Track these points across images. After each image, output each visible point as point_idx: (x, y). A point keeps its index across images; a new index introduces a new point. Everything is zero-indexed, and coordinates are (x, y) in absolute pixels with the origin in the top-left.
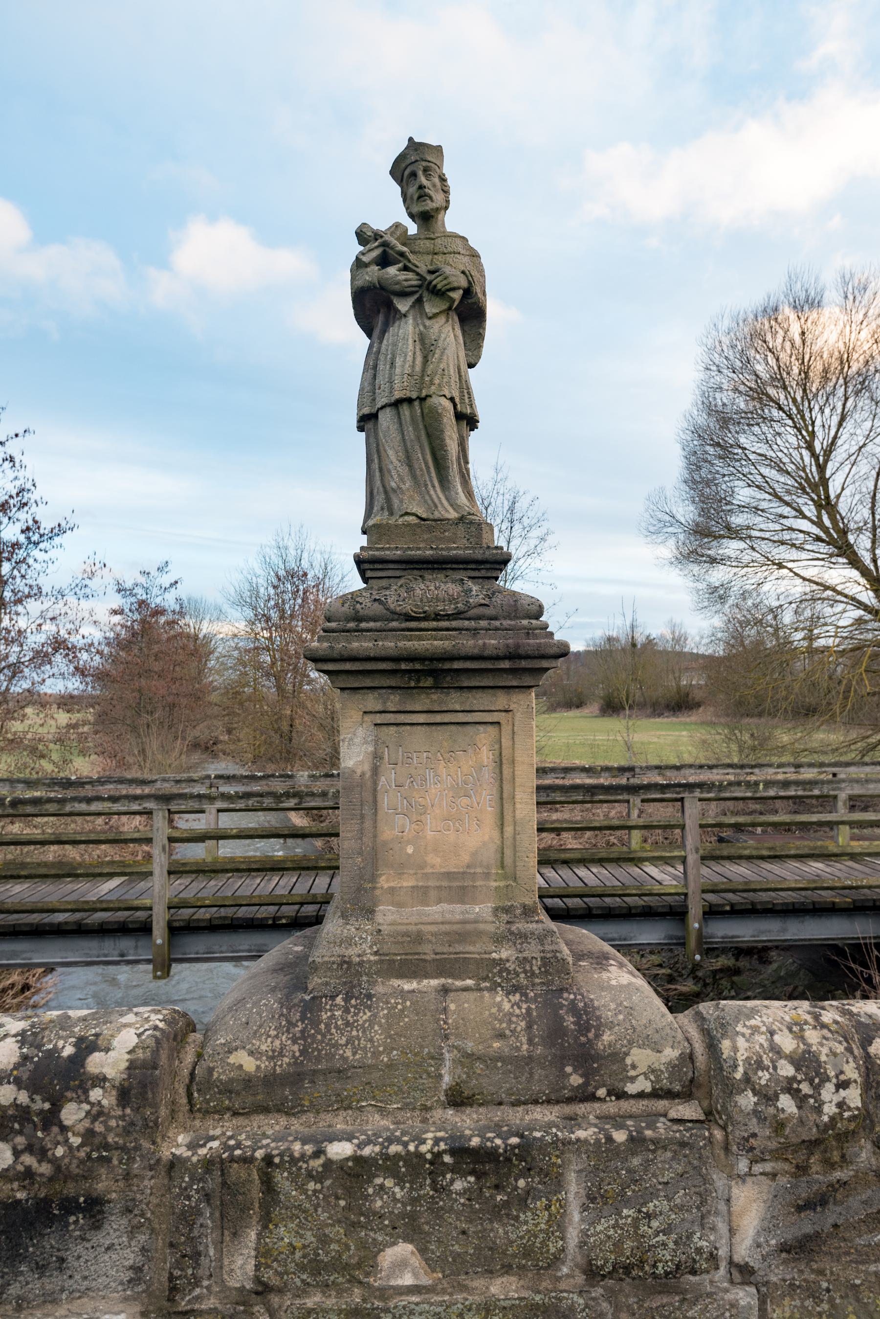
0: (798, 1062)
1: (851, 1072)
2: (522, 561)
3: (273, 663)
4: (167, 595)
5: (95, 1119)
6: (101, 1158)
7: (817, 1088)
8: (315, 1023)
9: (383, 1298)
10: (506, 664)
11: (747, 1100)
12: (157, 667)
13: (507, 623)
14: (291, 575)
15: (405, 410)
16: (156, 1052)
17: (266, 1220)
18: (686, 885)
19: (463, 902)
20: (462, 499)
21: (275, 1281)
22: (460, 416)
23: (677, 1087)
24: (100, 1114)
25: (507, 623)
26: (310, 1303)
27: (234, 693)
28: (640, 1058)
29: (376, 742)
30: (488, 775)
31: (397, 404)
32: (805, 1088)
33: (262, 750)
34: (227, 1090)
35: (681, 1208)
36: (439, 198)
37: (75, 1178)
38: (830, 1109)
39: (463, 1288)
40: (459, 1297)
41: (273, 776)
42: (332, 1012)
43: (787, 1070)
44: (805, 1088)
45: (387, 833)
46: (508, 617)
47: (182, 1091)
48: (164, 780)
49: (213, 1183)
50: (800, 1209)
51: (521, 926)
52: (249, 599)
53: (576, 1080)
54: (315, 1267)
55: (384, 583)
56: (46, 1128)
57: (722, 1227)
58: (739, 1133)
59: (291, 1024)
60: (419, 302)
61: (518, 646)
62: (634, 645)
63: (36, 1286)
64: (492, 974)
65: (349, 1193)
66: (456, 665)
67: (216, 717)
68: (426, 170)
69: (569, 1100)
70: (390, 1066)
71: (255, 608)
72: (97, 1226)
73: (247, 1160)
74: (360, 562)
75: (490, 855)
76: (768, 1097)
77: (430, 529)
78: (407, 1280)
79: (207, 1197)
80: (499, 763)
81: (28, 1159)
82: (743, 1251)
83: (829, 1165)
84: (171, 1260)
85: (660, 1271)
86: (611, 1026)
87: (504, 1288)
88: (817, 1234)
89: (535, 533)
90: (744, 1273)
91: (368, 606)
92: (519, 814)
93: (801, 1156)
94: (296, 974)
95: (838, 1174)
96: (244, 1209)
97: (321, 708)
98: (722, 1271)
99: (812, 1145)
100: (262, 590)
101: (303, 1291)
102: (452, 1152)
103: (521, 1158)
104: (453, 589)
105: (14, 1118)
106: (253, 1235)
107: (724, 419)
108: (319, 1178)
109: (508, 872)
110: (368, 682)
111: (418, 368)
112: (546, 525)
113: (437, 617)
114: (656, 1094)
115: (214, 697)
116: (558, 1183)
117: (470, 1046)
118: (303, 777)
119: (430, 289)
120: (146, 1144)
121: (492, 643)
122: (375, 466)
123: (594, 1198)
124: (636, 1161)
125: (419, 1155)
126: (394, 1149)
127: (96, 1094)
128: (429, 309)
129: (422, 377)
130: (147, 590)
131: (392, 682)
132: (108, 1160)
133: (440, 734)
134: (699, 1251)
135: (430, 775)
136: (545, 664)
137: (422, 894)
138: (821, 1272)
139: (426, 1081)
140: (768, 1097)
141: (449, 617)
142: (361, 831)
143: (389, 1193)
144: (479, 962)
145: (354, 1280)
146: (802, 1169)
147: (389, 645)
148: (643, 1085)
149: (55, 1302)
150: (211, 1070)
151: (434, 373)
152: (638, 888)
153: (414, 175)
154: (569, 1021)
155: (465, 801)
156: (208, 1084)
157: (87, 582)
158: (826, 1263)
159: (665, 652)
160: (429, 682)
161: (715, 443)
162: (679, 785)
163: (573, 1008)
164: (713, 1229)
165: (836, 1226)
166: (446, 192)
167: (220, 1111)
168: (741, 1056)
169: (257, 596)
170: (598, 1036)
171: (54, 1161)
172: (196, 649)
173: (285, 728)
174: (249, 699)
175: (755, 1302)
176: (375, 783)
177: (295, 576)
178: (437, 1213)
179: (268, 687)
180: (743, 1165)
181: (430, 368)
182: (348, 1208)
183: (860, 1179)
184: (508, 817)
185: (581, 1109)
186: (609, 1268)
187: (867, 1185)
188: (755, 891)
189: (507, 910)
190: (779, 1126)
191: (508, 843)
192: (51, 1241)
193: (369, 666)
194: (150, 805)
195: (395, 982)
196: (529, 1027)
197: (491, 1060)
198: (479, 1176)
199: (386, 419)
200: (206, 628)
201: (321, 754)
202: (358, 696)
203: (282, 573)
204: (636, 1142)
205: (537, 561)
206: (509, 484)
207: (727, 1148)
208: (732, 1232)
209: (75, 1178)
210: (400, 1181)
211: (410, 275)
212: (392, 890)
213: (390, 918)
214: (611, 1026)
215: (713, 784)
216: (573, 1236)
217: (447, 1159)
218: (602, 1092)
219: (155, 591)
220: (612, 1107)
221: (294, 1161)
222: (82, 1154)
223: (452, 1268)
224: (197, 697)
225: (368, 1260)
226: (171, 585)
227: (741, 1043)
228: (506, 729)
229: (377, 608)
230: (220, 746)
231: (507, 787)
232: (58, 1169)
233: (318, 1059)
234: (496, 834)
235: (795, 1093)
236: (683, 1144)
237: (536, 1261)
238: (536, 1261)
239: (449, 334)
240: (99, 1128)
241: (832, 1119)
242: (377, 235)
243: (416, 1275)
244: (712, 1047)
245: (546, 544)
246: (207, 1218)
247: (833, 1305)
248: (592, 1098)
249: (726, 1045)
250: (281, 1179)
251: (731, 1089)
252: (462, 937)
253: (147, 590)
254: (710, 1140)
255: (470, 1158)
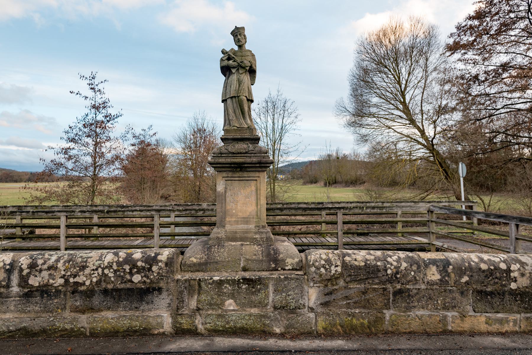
0: (326, 261)
1: (339, 263)
2: (288, 126)
3: (193, 165)
4: (152, 138)
5: (160, 270)
6: (161, 279)
7: (330, 267)
8: (211, 251)
9: (226, 312)
10: (258, 165)
11: (313, 269)
12: (148, 166)
13: (258, 155)
14: (200, 130)
15: (234, 99)
16: (173, 256)
17: (199, 294)
18: (338, 243)
19: (247, 224)
20: (249, 122)
21: (201, 307)
22: (248, 100)
23: (298, 268)
24: (161, 268)
25: (258, 155)
26: (209, 313)
27: (177, 177)
28: (289, 261)
29: (226, 184)
30: (254, 193)
31: (232, 98)
32: (327, 267)
33: (188, 198)
34: (190, 266)
35: (297, 294)
36: (243, 41)
37: (155, 283)
38: (333, 272)
39: (245, 310)
40: (244, 312)
41: (194, 205)
42: (215, 249)
43: (323, 262)
44: (327, 267)
45: (228, 207)
46: (259, 153)
47: (179, 266)
48: (156, 206)
49: (187, 285)
50: (325, 295)
51: (262, 230)
52: (183, 140)
53: (273, 266)
54: (210, 304)
55: (228, 144)
56: (149, 272)
57: (306, 299)
58: (311, 277)
59: (204, 252)
60: (238, 69)
61: (261, 161)
62: (338, 158)
63: (146, 307)
64: (254, 241)
65: (218, 288)
66: (246, 165)
67: (170, 186)
68: (240, 34)
69: (272, 270)
70: (228, 261)
71: (185, 143)
72: (160, 294)
73: (195, 280)
74: (222, 139)
75: (254, 213)
76: (318, 268)
77: (240, 130)
78: (232, 308)
79: (186, 288)
80: (257, 190)
81: (145, 279)
82: (311, 304)
83: (333, 285)
84: (177, 302)
85: (291, 308)
86: (282, 253)
87: (254, 311)
88: (330, 301)
89: (294, 115)
90: (312, 309)
91: (224, 151)
92: (261, 203)
93: (326, 283)
94: (205, 243)
95: (335, 287)
96: (194, 291)
97: (211, 182)
98: (306, 309)
99: (329, 280)
100: (188, 136)
101: (208, 310)
102: (242, 279)
103: (259, 281)
104: (245, 146)
105: (141, 269)
106: (196, 297)
107: (366, 71)
108: (211, 284)
109: (258, 217)
110: (224, 170)
111: (237, 88)
112: (297, 112)
113: (241, 153)
114: (293, 270)
115: (169, 178)
116: (267, 287)
117: (248, 257)
118: (205, 205)
119: (240, 66)
120: (171, 276)
121: (255, 160)
122: (226, 113)
123: (276, 291)
124: (286, 283)
125: (235, 280)
126: (229, 278)
127: (160, 264)
128: (241, 71)
129: (238, 90)
130: (144, 137)
131: (230, 170)
132: (163, 279)
133: (242, 182)
134: (301, 304)
135: (239, 193)
136: (268, 165)
137: (237, 222)
138: (330, 310)
139: (237, 265)
140: (318, 268)
141: (244, 153)
142: (222, 207)
143: (227, 288)
144: (251, 238)
145: (219, 308)
146: (326, 286)
147: (229, 160)
148: (290, 267)
149: (151, 311)
150: (186, 262)
151: (241, 89)
152: (321, 243)
153: (237, 35)
154: (272, 252)
155: (248, 199)
156: (185, 265)
157: (126, 135)
158: (331, 308)
159: (351, 161)
160: (239, 170)
161: (363, 81)
162: (336, 208)
163: (273, 249)
164: (304, 299)
165: (334, 299)
166: (245, 39)
167: (188, 271)
168: (312, 259)
169: (186, 139)
170: (279, 255)
171: (150, 279)
172: (162, 159)
173: (197, 189)
174: (183, 179)
175: (314, 317)
176: (225, 195)
177: (201, 130)
178: (239, 293)
179: (191, 175)
180: (312, 284)
181: (240, 88)
182: (218, 291)
183: (340, 288)
184: (259, 204)
185: (274, 272)
186: (279, 307)
187: (342, 290)
188: (362, 245)
189: (258, 227)
190: (321, 275)
191: (259, 210)
192: (150, 297)
193: (224, 166)
194: (153, 213)
195: (230, 243)
196: (262, 253)
197: (253, 261)
198: (249, 285)
199: (229, 101)
200: (166, 151)
201: (211, 199)
202: (221, 173)
203: (196, 130)
204: (286, 278)
205: (294, 126)
206: (283, 96)
207: (308, 280)
208: (309, 300)
209: (155, 283)
210: (230, 285)
211: (235, 63)
212: (229, 221)
213: (229, 228)
214: (282, 253)
215: (348, 207)
216: (271, 299)
217: (241, 281)
218: (280, 269)
219: (148, 137)
220: (282, 272)
221: (205, 280)
222: (157, 278)
223: (243, 306)
224: (163, 177)
225: (223, 303)
226: (154, 134)
227: (313, 256)
228: (258, 181)
229: (226, 151)
230: (171, 198)
231: (258, 196)
232: (151, 281)
233: (211, 259)
234: (256, 208)
235: (325, 268)
236: (297, 279)
237: (262, 305)
238: (262, 305)
239: (246, 78)
240: (161, 272)
241: (334, 274)
242: (227, 53)
243: (234, 307)
244: (306, 258)
245: (298, 119)
246: (186, 293)
247: (333, 318)
248: (277, 270)
249: (309, 257)
250: (203, 284)
251: (310, 266)
252: (247, 232)
253: (144, 137)
254: (304, 278)
255: (246, 281)
